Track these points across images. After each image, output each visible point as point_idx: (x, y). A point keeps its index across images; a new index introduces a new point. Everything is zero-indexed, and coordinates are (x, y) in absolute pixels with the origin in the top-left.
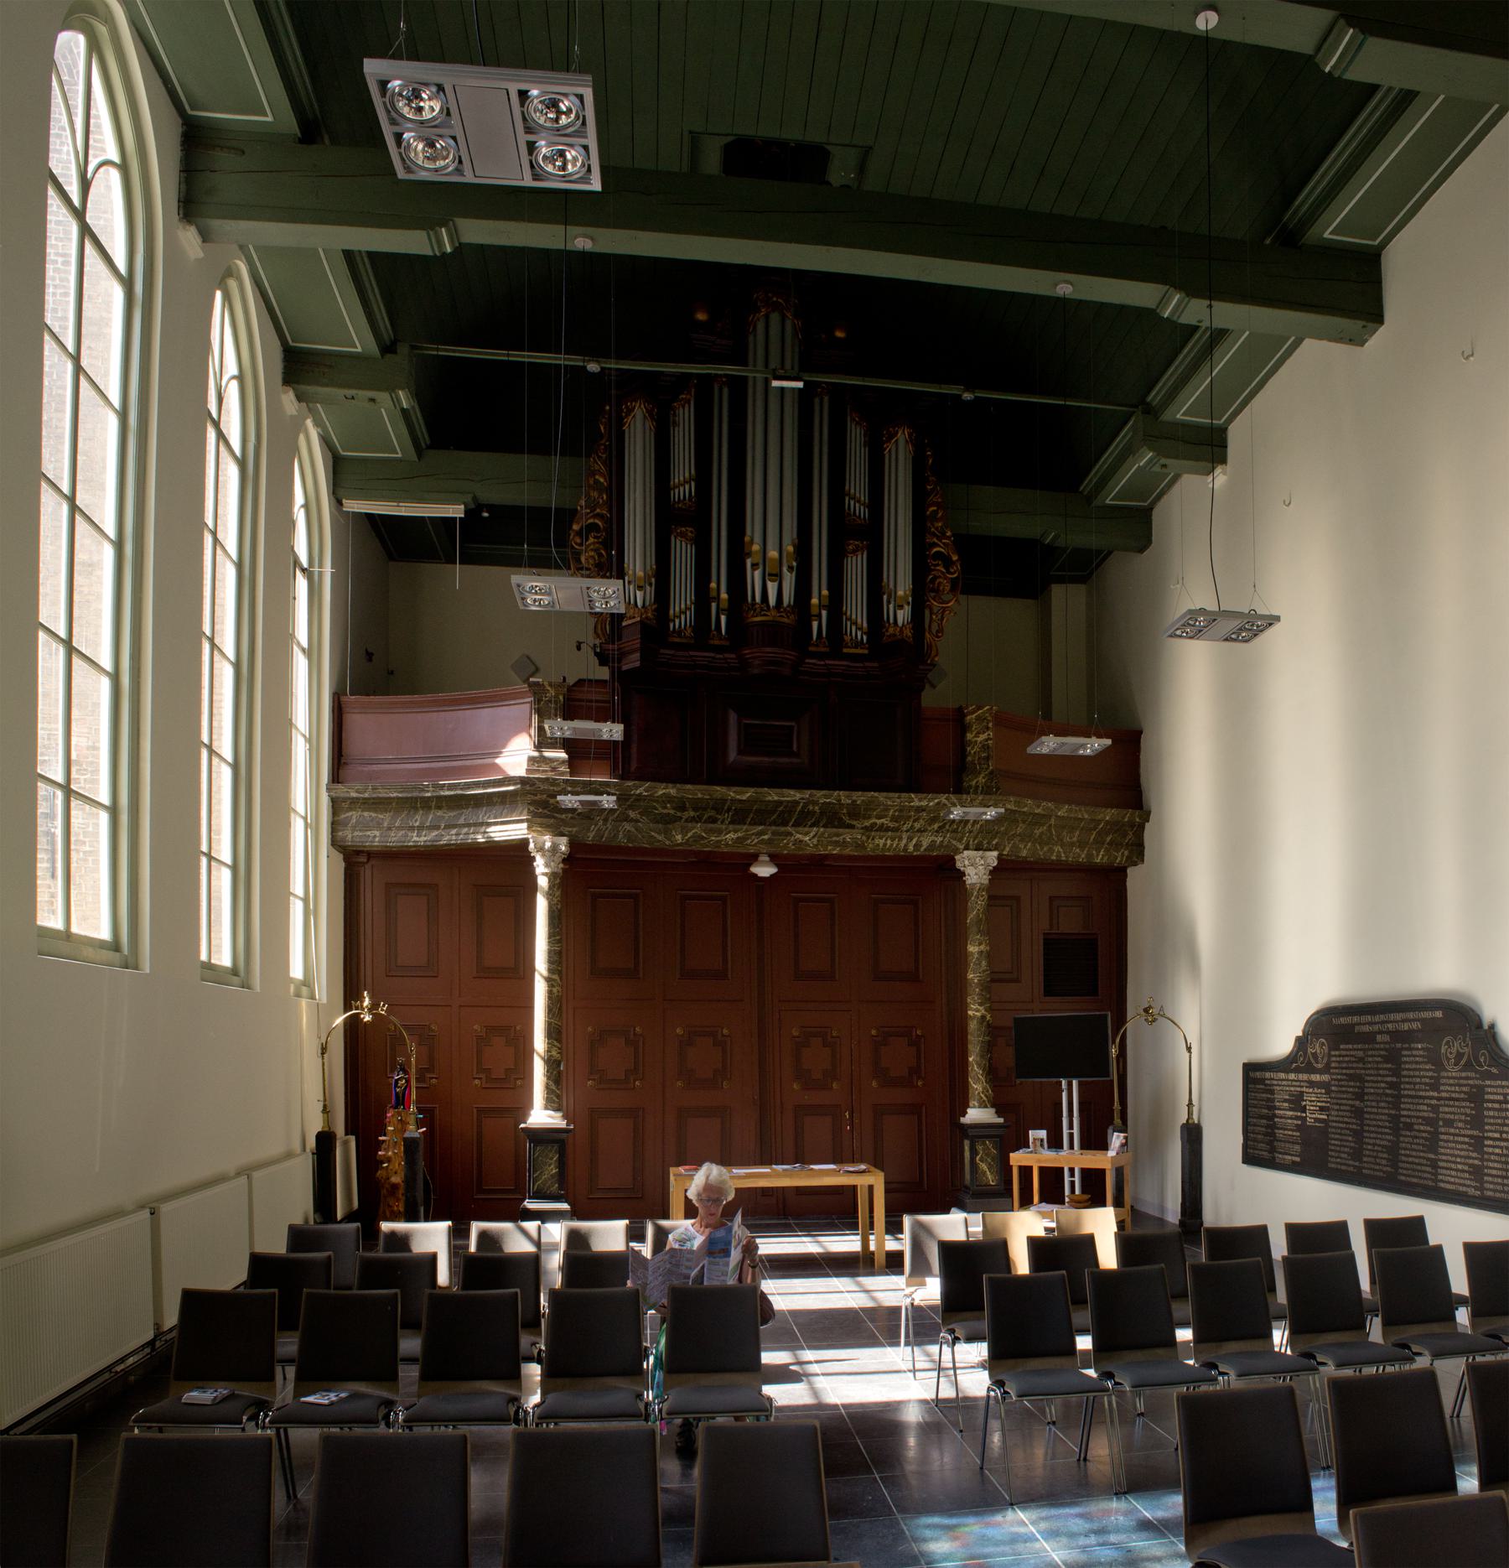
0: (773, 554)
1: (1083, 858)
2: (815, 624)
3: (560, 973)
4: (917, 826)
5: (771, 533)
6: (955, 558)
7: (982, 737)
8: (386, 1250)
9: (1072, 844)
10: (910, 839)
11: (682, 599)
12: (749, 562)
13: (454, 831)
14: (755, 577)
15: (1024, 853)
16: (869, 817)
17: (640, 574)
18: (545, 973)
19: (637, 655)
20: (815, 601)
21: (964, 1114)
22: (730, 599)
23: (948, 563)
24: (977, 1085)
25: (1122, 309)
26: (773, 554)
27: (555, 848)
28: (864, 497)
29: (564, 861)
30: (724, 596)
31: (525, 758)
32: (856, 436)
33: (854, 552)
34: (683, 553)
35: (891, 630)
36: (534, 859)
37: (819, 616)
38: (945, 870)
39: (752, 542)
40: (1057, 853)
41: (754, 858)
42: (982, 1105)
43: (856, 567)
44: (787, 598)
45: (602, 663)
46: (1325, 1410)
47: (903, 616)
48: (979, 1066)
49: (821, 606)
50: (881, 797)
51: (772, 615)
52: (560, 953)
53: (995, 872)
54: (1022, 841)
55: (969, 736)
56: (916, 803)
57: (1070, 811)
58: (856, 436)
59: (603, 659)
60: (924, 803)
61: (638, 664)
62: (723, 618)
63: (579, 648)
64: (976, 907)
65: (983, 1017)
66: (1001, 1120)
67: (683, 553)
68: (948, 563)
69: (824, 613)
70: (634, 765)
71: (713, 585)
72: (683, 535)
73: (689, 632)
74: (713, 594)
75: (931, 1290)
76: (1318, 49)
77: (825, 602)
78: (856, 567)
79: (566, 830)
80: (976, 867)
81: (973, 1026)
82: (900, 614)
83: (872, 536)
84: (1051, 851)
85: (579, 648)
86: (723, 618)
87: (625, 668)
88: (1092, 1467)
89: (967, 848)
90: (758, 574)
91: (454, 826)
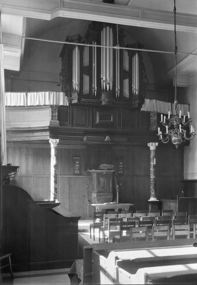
2: (117, 94)
5: (107, 76)
7: (154, 118)
11: (86, 89)
18: (54, 192)
19: (77, 100)
20: (117, 89)
21: (149, 199)
22: (97, 88)
27: (56, 142)
28: (128, 67)
29: (57, 144)
30: (96, 87)
31: (49, 121)
34: (86, 78)
37: (118, 92)
42: (154, 197)
43: (126, 82)
48: (153, 189)
49: (118, 90)
52: (57, 164)
61: (77, 102)
62: (96, 92)
64: (152, 155)
65: (154, 178)
66: (158, 200)
67: (86, 78)
69: (119, 92)
70: (74, 123)
71: (93, 85)
74: (93, 87)
75: (160, 210)
76: (172, 112)
77: (119, 89)
78: (126, 82)
81: (152, 180)
86: (96, 92)
87: (73, 103)
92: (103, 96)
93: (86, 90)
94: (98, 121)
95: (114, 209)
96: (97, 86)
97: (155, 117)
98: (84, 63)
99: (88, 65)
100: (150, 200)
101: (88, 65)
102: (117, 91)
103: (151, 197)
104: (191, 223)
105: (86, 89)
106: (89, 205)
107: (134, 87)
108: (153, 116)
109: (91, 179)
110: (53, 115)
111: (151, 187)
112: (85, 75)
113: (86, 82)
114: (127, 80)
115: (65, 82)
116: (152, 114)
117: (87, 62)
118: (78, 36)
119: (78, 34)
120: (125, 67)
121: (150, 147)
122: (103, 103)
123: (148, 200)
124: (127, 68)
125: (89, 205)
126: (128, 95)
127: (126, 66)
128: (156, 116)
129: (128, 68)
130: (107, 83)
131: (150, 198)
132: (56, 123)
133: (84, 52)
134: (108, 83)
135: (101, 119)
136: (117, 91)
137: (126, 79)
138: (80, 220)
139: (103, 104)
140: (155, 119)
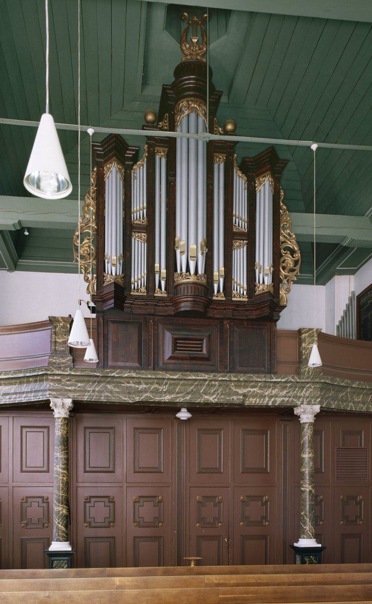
0: (192, 246)
1: (364, 409)
6: (296, 249)
8: (92, 145)
9: (359, 402)
10: (270, 397)
13: (8, 397)
15: (333, 407)
17: (114, 258)
19: (112, 301)
20: (216, 273)
21: (297, 541)
23: (292, 252)
24: (308, 527)
25: (10, 125)
28: (245, 216)
30: (164, 271)
33: (239, 247)
34: (139, 246)
35: (261, 287)
37: (219, 281)
39: (180, 240)
40: (351, 406)
43: (240, 255)
44: (201, 271)
45: (93, 312)
47: (268, 280)
50: (255, 378)
51: (192, 279)
53: (317, 416)
54: (332, 400)
55: (304, 345)
56: (275, 380)
57: (359, 384)
59: (93, 310)
65: (310, 491)
66: (320, 545)
67: (139, 246)
69: (222, 280)
72: (141, 238)
73: (143, 289)
74: (157, 269)
76: (235, 71)
78: (240, 255)
80: (307, 414)
82: (266, 278)
83: (250, 237)
84: (347, 405)
91: (8, 394)
93: (139, 276)
95: (176, 138)
96: (167, 268)
100: (299, 543)
103: (301, 536)
104: (195, 257)
106: (206, 15)
111: (302, 513)
113: (243, 209)
116: (307, 334)
121: (301, 417)
123: (295, 545)
124: (242, 219)
125: (206, 15)
128: (316, 339)
130: (189, 257)
131: (300, 539)
134: (191, 257)
135: (176, 350)
136: (216, 277)
139: (183, 309)
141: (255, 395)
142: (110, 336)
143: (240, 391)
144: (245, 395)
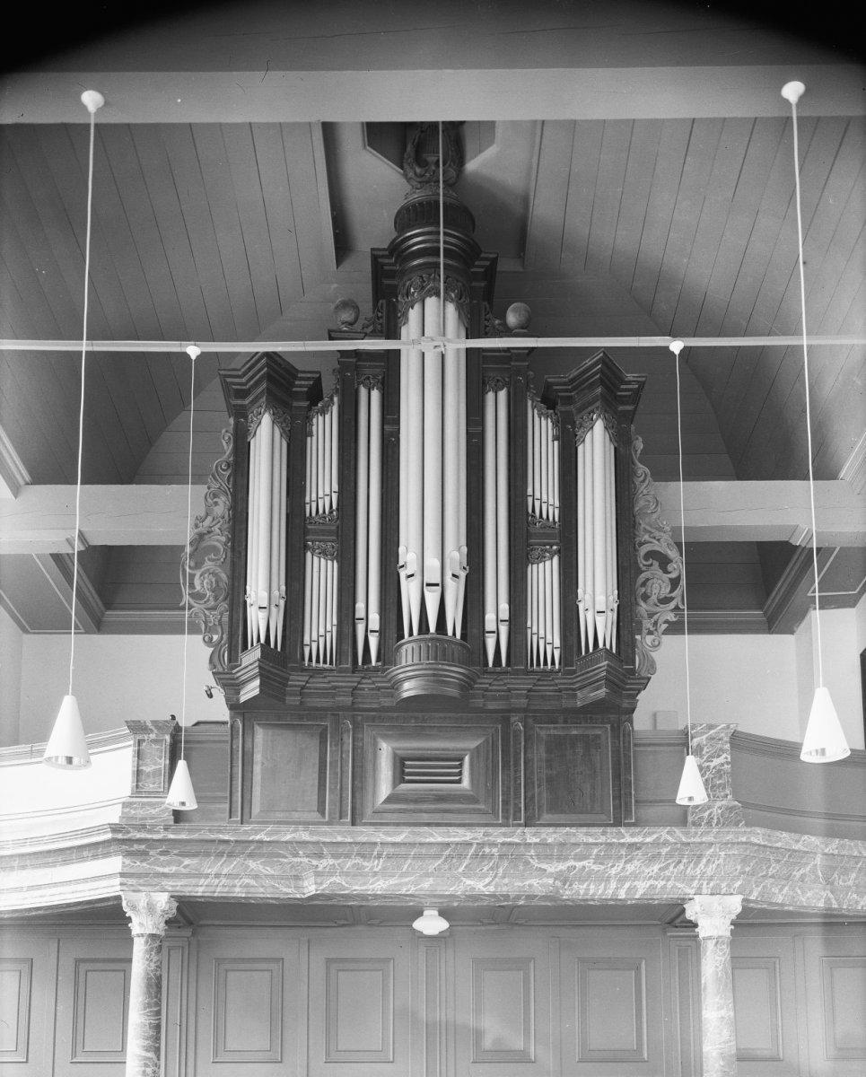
3: (157, 1051)
4: (630, 868)
7: (716, 762)
10: (622, 880)
11: (320, 627)
12: (403, 574)
14: (410, 593)
15: (779, 899)
16: (566, 859)
19: (257, 682)
20: (490, 617)
26: (432, 562)
28: (555, 500)
32: (542, 432)
34: (322, 573)
36: (129, 919)
38: (671, 920)
41: (418, 913)
43: (544, 576)
46: (197, 892)
56: (628, 839)
58: (542, 432)
60: (635, 840)
62: (374, 642)
63: (210, 696)
67: (322, 573)
68: (664, 561)
69: (504, 629)
70: (256, 809)
72: (324, 553)
77: (505, 615)
78: (544, 576)
79: (168, 884)
80: (713, 917)
83: (565, 539)
85: (210, 696)
87: (243, 699)
88: (310, 509)
89: (699, 892)
90: (535, 637)
92: (409, 653)
94: (384, 788)
97: (722, 751)
98: (314, 496)
99: (334, 507)
101: (334, 507)
102: (494, 629)
105: (320, 627)
107: (587, 597)
108: (705, 750)
109: (439, 301)
110: (144, 768)
112: (316, 559)
114: (548, 563)
115: (208, 600)
117: (328, 492)
118: (311, 383)
119: (264, 361)
120: (537, 504)
122: (409, 689)
126: (557, 643)
127: (544, 493)
128: (727, 746)
129: (557, 504)
132: (153, 812)
133: (311, 443)
136: (490, 624)
137: (541, 559)
138: (470, 160)
139: (405, 695)
140: (722, 765)
141: (585, 876)
142: (258, 757)
143: (553, 868)
144: (564, 878)
